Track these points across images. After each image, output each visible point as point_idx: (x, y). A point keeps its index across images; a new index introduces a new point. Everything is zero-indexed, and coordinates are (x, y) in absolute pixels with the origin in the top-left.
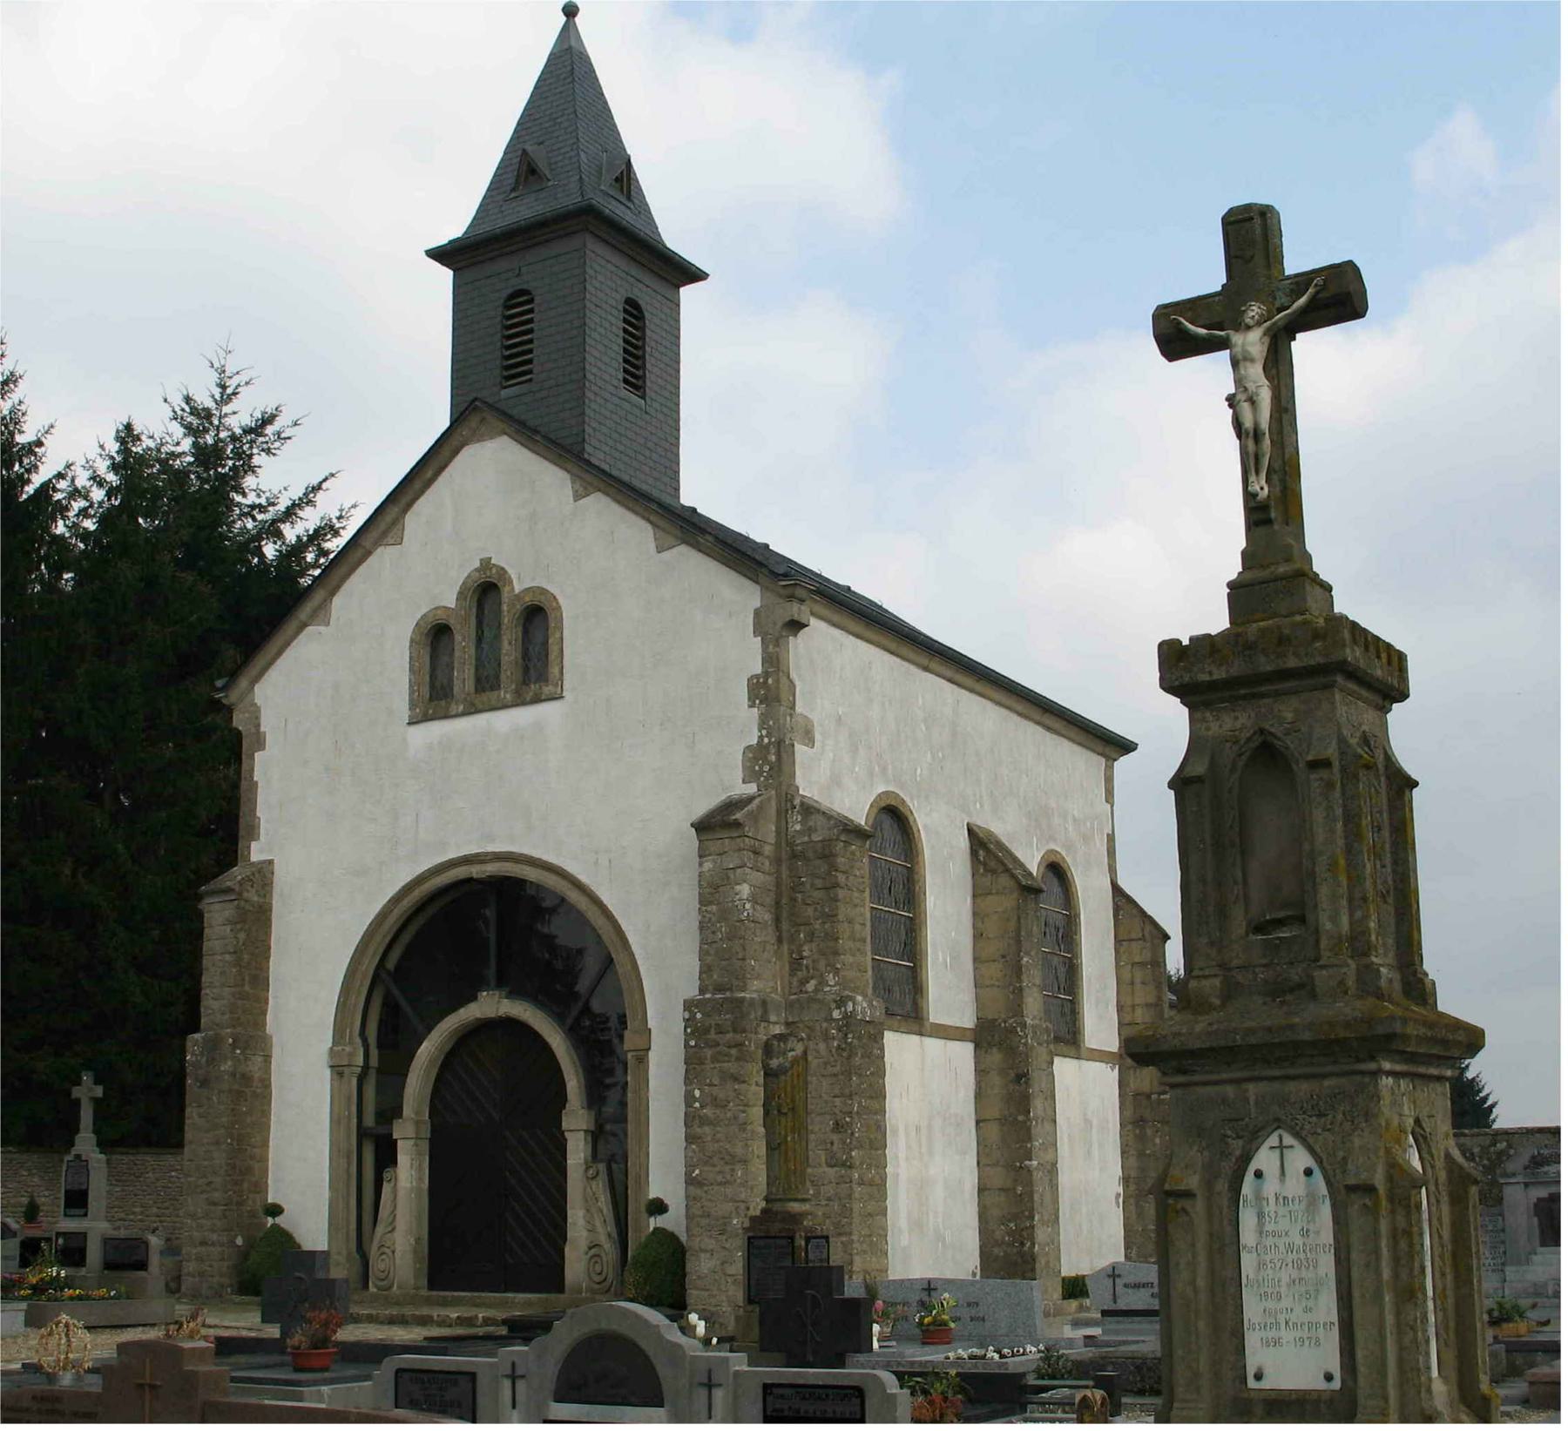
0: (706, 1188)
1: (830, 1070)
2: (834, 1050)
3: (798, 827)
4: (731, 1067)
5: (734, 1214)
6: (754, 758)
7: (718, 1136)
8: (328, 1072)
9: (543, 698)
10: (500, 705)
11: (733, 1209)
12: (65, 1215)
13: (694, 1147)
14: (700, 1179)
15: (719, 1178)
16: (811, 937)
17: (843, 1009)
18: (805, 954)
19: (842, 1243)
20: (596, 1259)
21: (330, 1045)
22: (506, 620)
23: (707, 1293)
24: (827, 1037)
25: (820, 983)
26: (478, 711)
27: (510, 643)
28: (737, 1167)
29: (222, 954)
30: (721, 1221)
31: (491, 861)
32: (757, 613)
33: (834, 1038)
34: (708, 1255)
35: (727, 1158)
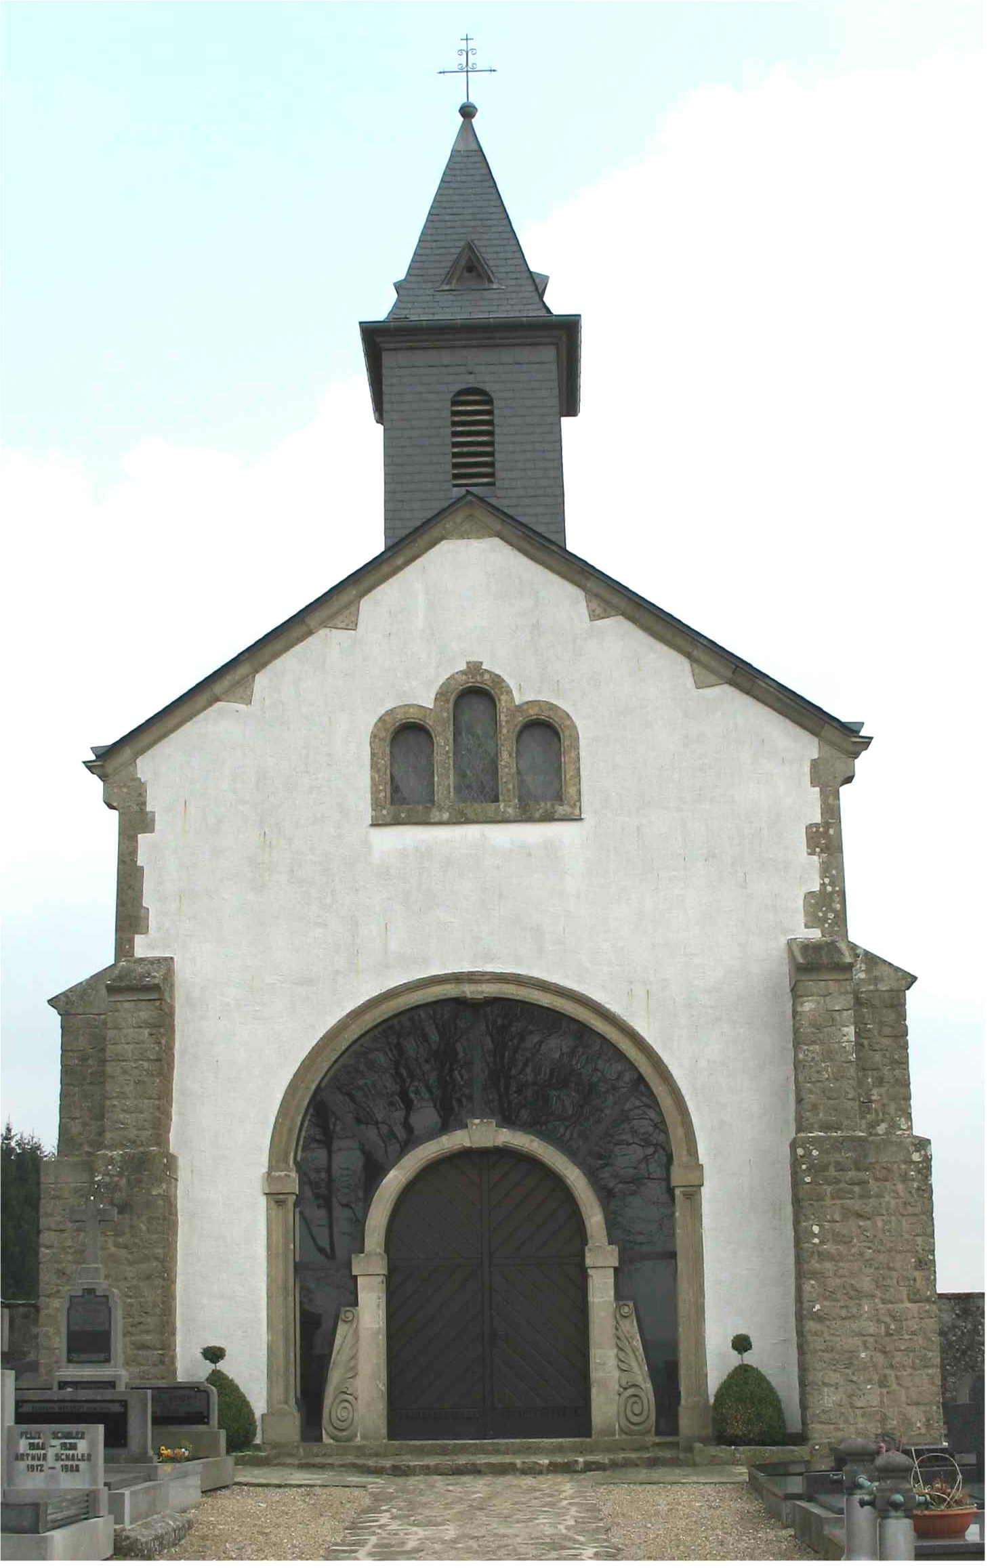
0: (828, 1323)
1: (910, 1210)
2: (914, 1191)
3: (862, 975)
4: (856, 1205)
5: (861, 1349)
6: (817, 904)
7: (841, 1272)
8: (263, 1201)
9: (556, 817)
10: (499, 818)
11: (860, 1343)
12: (69, 1361)
13: (813, 1282)
14: (821, 1313)
15: (844, 1313)
16: (880, 1082)
17: (923, 1152)
18: (873, 1098)
19: (928, 1375)
20: (634, 1399)
21: (265, 1170)
22: (505, 731)
23: (832, 1427)
24: (905, 1178)
25: (890, 1126)
26: (468, 821)
27: (510, 755)
28: (864, 1301)
29: (136, 1060)
30: (847, 1355)
31: (488, 981)
32: (815, 764)
33: (913, 1180)
34: (832, 1389)
35: (852, 1293)
